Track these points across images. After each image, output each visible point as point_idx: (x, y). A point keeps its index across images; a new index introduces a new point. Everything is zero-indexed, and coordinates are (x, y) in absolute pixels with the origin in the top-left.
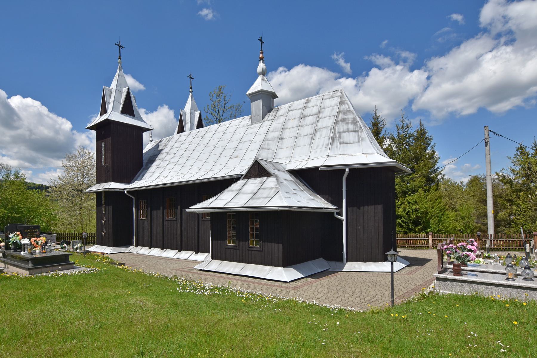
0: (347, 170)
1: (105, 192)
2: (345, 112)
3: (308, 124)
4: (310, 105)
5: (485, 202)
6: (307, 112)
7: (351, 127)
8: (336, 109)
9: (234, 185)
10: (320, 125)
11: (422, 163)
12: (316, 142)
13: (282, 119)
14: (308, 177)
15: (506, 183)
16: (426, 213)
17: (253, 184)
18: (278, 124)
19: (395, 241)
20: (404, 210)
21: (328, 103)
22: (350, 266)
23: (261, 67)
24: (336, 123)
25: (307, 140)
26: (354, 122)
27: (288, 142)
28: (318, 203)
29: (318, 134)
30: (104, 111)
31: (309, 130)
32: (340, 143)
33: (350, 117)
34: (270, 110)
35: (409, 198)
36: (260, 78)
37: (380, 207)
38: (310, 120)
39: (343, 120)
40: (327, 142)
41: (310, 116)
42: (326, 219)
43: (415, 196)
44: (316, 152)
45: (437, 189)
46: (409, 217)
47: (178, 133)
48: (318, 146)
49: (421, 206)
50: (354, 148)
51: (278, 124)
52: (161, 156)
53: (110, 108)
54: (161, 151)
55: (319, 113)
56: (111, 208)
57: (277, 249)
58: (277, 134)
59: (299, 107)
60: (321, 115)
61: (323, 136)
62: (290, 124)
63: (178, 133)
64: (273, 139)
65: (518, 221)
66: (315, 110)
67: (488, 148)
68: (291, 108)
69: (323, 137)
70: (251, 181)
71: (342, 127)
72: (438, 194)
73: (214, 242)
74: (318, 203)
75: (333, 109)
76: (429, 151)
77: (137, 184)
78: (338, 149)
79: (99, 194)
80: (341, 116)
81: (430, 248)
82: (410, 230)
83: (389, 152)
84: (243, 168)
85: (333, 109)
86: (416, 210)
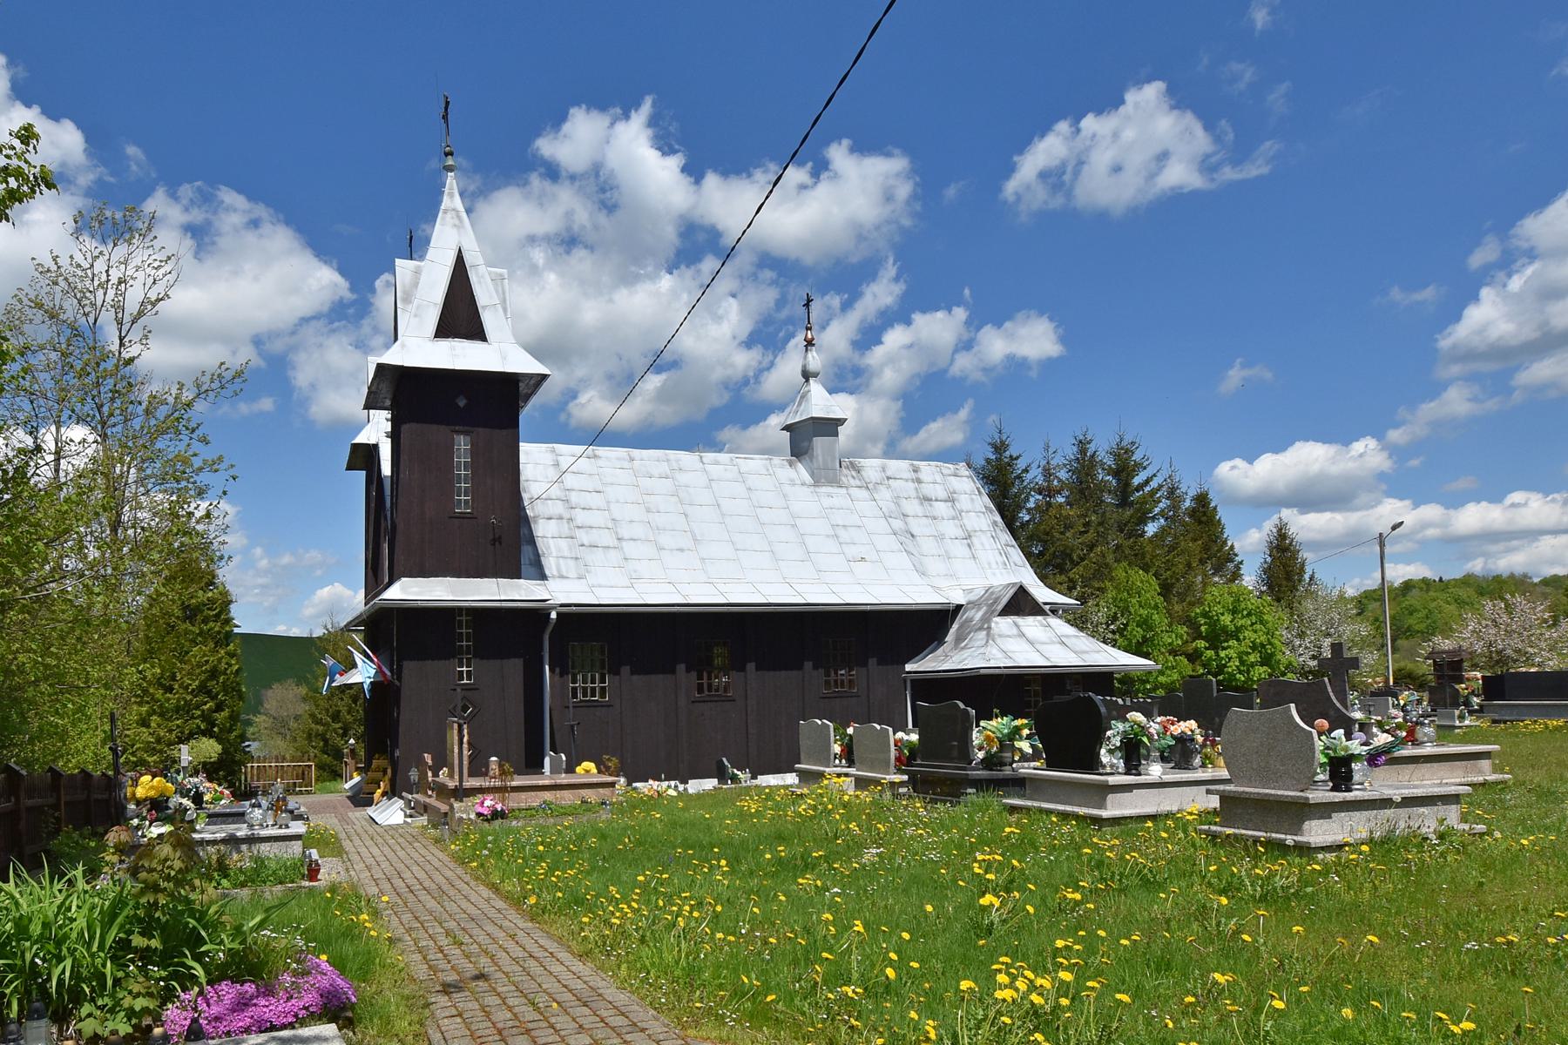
68: (889, 473)
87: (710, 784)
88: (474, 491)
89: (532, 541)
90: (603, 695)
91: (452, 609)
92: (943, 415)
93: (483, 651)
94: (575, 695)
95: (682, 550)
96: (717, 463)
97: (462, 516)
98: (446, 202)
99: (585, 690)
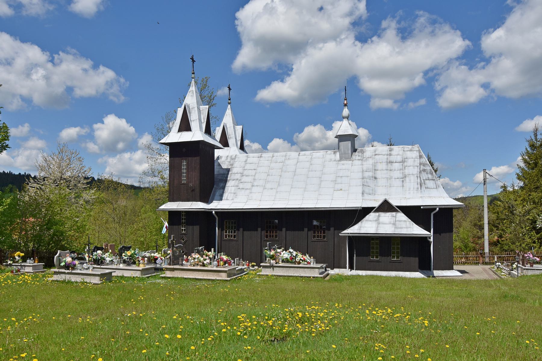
0: (438, 209)
1: (185, 212)
2: (424, 165)
3: (396, 169)
4: (393, 153)
6: (392, 158)
7: (430, 176)
8: (418, 161)
9: (368, 216)
10: (407, 171)
12: (407, 184)
13: (371, 161)
14: (415, 213)
17: (386, 217)
18: (368, 164)
21: (409, 154)
22: (436, 273)
24: (420, 172)
25: (399, 183)
27: (381, 182)
28: (417, 230)
29: (407, 179)
30: (185, 126)
32: (426, 188)
34: (355, 150)
38: (396, 166)
40: (417, 186)
41: (396, 162)
42: (424, 240)
44: (410, 193)
48: (410, 189)
50: (434, 192)
51: (368, 164)
53: (194, 125)
54: (228, 170)
56: (197, 228)
58: (371, 174)
59: (384, 153)
60: (405, 164)
61: (412, 181)
62: (379, 166)
64: (369, 178)
65: (503, 243)
66: (399, 159)
67: (485, 186)
68: (377, 153)
70: (382, 214)
73: (360, 258)
74: (417, 230)
75: (415, 161)
79: (174, 217)
84: (376, 205)
85: (415, 161)
87: (418, 275)
88: (187, 177)
89: (224, 188)
90: (235, 237)
91: (181, 211)
92: (284, 140)
93: (188, 224)
94: (226, 237)
95: (272, 189)
96: (305, 155)
97: (184, 184)
98: (191, 89)
99: (229, 235)
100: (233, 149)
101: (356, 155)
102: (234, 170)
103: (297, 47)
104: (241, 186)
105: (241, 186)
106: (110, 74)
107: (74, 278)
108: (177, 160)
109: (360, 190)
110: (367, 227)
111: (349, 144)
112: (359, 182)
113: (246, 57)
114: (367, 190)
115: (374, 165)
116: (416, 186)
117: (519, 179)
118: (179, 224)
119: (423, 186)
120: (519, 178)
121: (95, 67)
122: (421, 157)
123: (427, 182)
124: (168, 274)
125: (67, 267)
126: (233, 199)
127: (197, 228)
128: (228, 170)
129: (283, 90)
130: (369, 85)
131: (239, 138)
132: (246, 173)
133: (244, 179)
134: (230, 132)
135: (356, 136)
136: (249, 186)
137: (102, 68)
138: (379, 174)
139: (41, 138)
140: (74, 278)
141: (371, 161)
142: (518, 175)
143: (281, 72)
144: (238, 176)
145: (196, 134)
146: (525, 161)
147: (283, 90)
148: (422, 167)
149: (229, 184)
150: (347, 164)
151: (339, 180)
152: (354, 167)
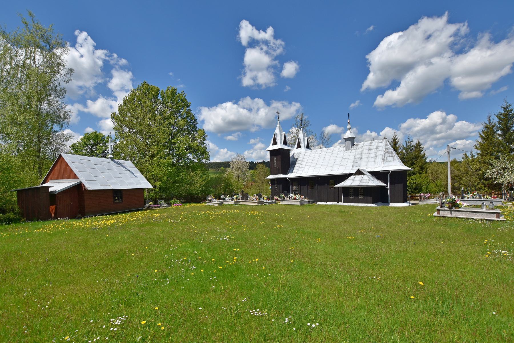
2: (388, 149)
4: (372, 144)
5: (447, 178)
6: (371, 147)
7: (390, 155)
8: (384, 147)
10: (378, 153)
11: (419, 160)
12: (377, 160)
13: (360, 150)
14: (376, 174)
15: (458, 170)
16: (420, 184)
17: (358, 177)
18: (359, 151)
19: (407, 197)
20: (410, 183)
21: (380, 144)
22: (391, 204)
23: (349, 126)
24: (385, 153)
25: (373, 159)
26: (392, 153)
27: (364, 160)
28: (379, 183)
29: (377, 157)
30: (275, 143)
31: (373, 155)
33: (390, 151)
34: (354, 145)
35: (412, 177)
36: (349, 131)
37: (402, 185)
38: (373, 151)
39: (387, 152)
43: (415, 176)
45: (426, 172)
46: (412, 186)
47: (297, 148)
49: (418, 181)
50: (392, 163)
51: (359, 151)
52: (297, 162)
53: (278, 142)
54: (297, 159)
55: (377, 148)
56: (281, 186)
57: (370, 198)
58: (359, 156)
62: (364, 152)
63: (297, 148)
64: (358, 158)
66: (375, 147)
69: (380, 159)
70: (357, 176)
71: (387, 155)
72: (426, 175)
74: (379, 183)
76: (422, 153)
77: (290, 175)
78: (386, 164)
79: (272, 180)
80: (386, 150)
81: (263, 51)
82: (412, 192)
83: (403, 160)
84: (354, 171)
86: (415, 183)
89: (294, 167)
93: (278, 184)
100: (303, 149)
101: (354, 148)
102: (299, 159)
103: (406, 68)
104: (301, 166)
105: (301, 166)
106: (298, 105)
107: (211, 204)
108: (272, 157)
109: (352, 164)
110: (347, 183)
111: (350, 142)
112: (352, 161)
113: (371, 80)
114: (355, 164)
115: (362, 152)
116: (381, 161)
117: (476, 148)
118: (274, 184)
119: (386, 160)
120: (476, 148)
121: (290, 103)
122: (386, 145)
123: (388, 158)
124: (241, 203)
125: (210, 201)
126: (297, 172)
127: (281, 186)
128: (297, 159)
129: (393, 96)
130: (458, 82)
131: (306, 143)
132: (304, 160)
133: (303, 163)
134: (302, 141)
135: (355, 138)
136: (304, 166)
137: (293, 103)
138: (363, 156)
139: (263, 143)
140: (211, 204)
141: (360, 150)
142: (476, 146)
143: (395, 85)
144: (300, 162)
145: (280, 145)
146: (482, 137)
147: (393, 96)
148: (386, 150)
149: (296, 166)
150: (349, 152)
151: (343, 160)
152: (353, 152)
